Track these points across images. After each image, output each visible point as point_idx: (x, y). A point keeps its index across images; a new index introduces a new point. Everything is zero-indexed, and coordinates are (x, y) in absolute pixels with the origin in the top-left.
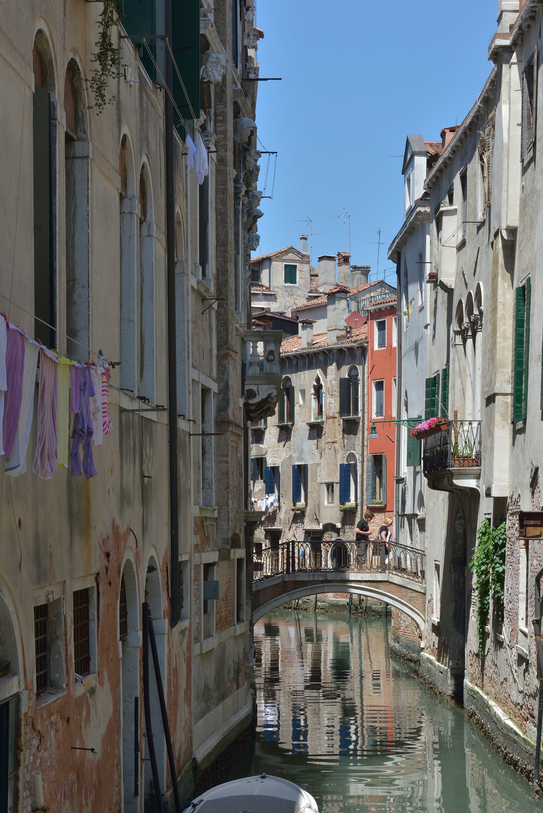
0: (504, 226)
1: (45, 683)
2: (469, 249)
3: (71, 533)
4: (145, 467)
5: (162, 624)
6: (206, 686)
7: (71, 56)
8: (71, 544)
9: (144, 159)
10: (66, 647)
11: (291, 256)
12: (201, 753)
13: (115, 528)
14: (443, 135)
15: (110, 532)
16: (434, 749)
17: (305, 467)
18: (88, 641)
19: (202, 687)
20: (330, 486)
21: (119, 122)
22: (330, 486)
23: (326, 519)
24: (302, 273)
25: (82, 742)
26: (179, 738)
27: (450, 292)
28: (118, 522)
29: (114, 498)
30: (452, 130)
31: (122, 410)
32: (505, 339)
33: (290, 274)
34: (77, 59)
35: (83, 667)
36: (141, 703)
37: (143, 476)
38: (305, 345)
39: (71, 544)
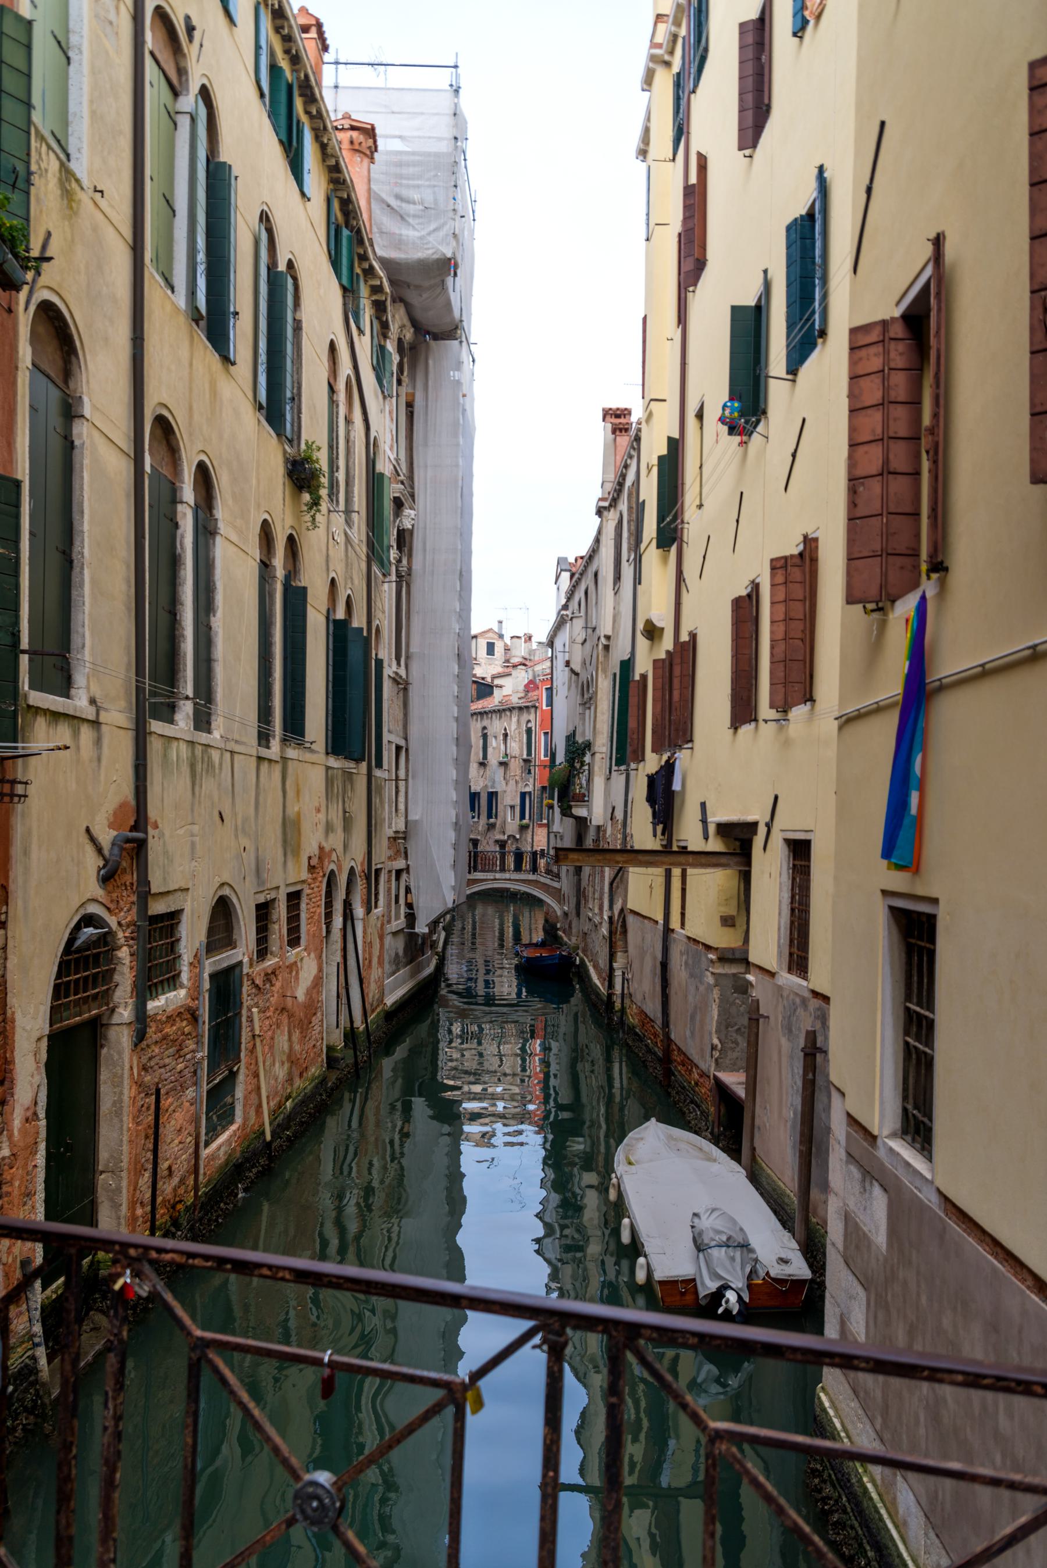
0: (602, 635)
1: (262, 952)
2: (588, 644)
3: (285, 855)
4: (347, 805)
5: (359, 911)
6: (397, 954)
7: (290, 531)
8: (285, 862)
9: (349, 592)
10: (279, 928)
11: (490, 635)
12: (390, 1000)
13: (321, 848)
14: (576, 560)
15: (317, 852)
16: (476, 982)
17: (496, 793)
18: (210, 923)
19: (393, 955)
20: (512, 807)
21: (328, 569)
22: (512, 807)
23: (509, 832)
24: (499, 649)
25: (293, 992)
26: (372, 990)
27: (577, 674)
28: (324, 844)
29: (321, 828)
30: (582, 558)
31: (328, 768)
32: (603, 714)
33: (491, 648)
34: (294, 533)
35: (294, 941)
36: (342, 967)
37: (345, 812)
38: (497, 703)
39: (285, 862)
